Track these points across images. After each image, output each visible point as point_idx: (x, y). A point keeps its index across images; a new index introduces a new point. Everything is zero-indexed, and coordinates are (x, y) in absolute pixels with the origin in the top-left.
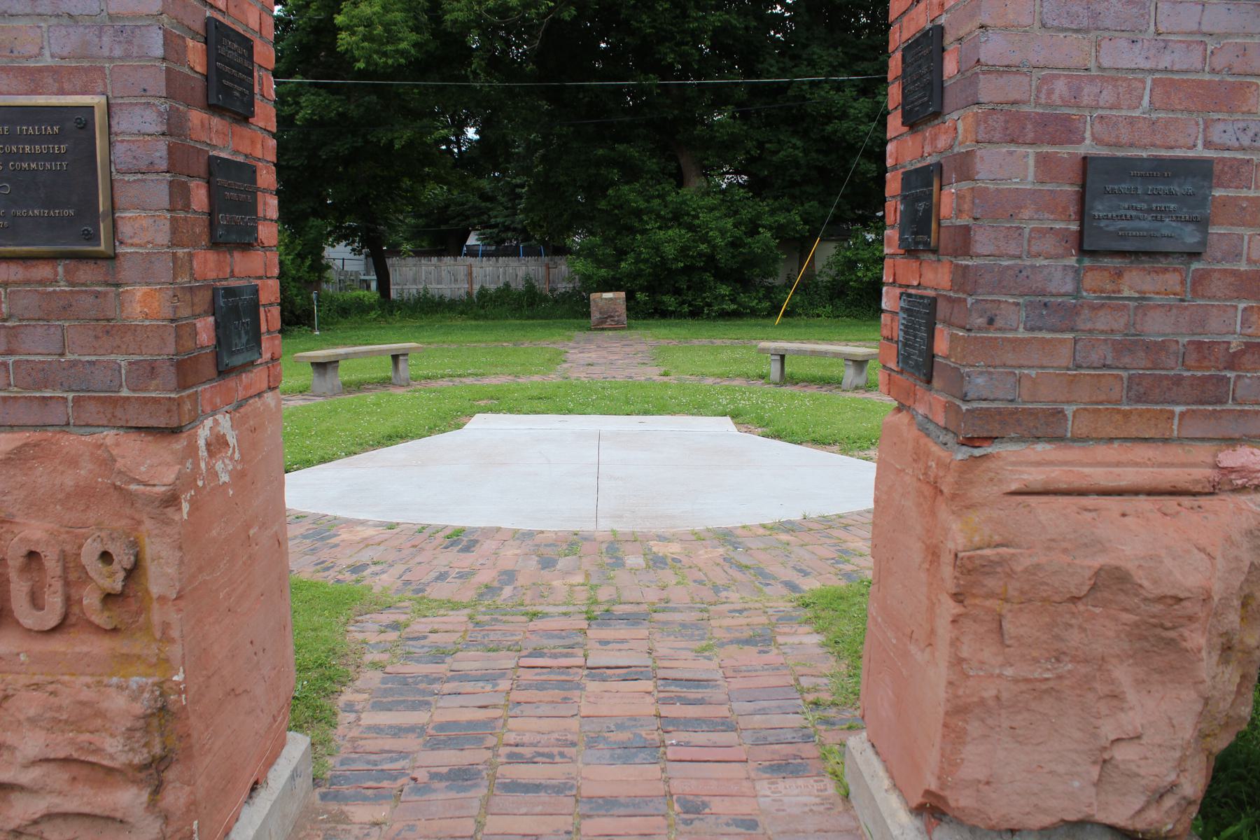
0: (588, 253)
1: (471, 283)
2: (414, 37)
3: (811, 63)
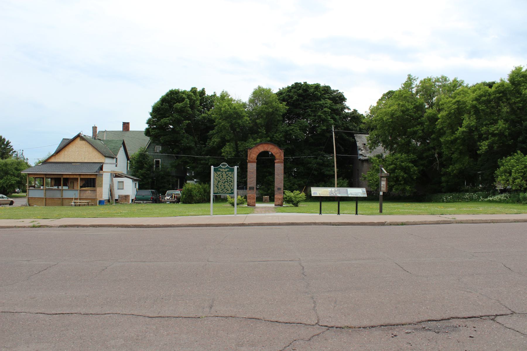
2: (234, 153)
3: (304, 153)
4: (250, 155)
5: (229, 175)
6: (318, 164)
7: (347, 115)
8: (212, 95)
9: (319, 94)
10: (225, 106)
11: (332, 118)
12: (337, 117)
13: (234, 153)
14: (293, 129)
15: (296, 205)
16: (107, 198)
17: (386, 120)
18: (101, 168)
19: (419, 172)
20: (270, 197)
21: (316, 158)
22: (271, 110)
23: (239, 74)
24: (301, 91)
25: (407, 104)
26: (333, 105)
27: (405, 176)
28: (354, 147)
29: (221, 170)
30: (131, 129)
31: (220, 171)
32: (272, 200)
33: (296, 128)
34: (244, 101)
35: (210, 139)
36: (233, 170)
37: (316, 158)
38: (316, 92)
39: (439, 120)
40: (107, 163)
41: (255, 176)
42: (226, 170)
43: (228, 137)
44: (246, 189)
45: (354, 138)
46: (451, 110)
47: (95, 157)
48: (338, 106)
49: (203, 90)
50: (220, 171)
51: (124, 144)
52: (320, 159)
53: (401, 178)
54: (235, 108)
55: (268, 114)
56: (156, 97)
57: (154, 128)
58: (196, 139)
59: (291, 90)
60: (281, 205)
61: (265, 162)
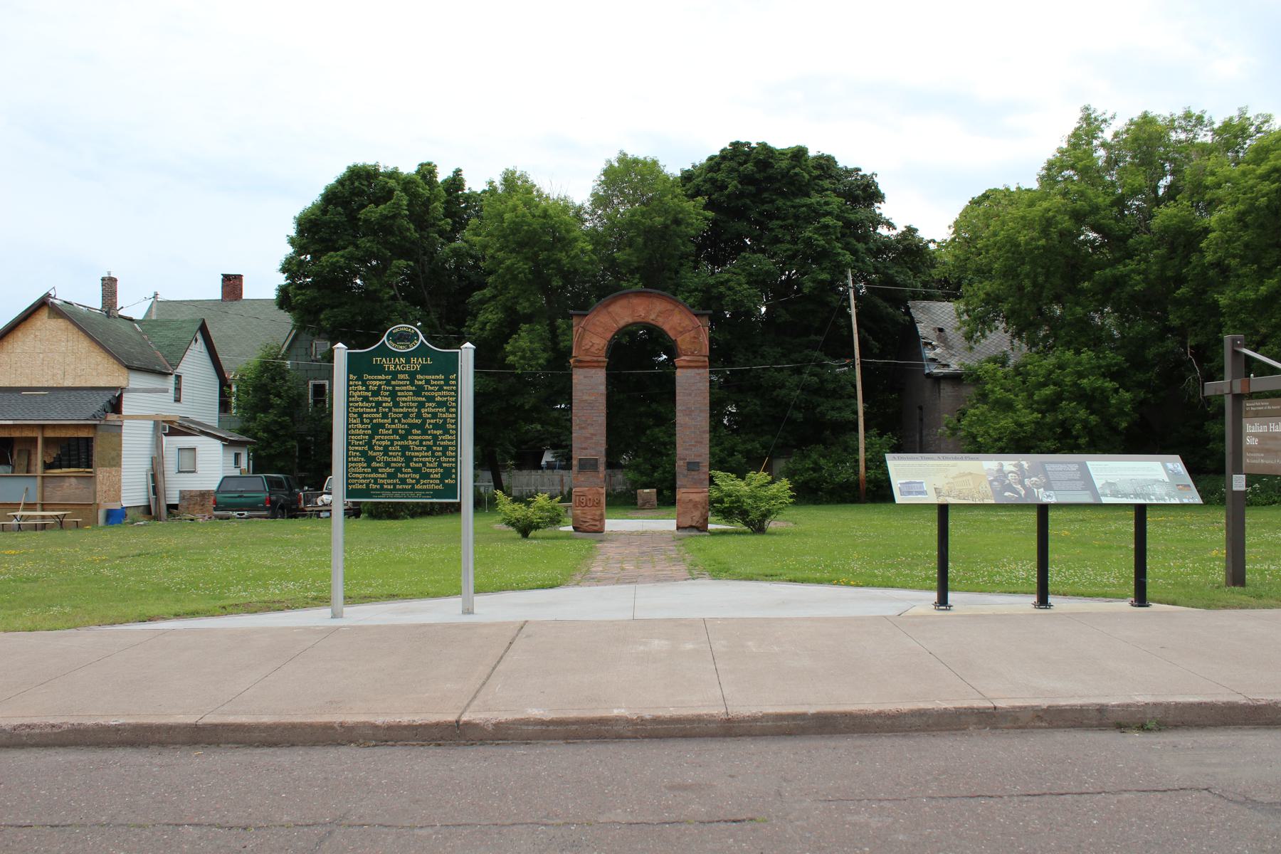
0: (636, 468)
1: (562, 485)
2: (545, 355)
3: (763, 357)
4: (582, 337)
5: (431, 390)
6: (805, 388)
7: (886, 245)
8: (484, 192)
9: (807, 176)
10: (514, 209)
11: (847, 247)
12: (861, 246)
13: (545, 355)
14: (728, 281)
15: (758, 527)
16: (143, 502)
17: (1027, 243)
18: (116, 406)
19: (1134, 409)
20: (659, 493)
21: (798, 371)
22: (659, 220)
23: (557, 112)
24: (750, 166)
25: (1090, 192)
26: (846, 211)
27: (1093, 419)
28: (908, 339)
29: (388, 364)
30: (247, 293)
31: (380, 370)
32: (667, 499)
33: (735, 278)
34: (578, 203)
35: (475, 316)
36: (450, 367)
37: (798, 371)
38: (797, 170)
39: (1212, 236)
40: (135, 390)
41: (602, 419)
42: (416, 363)
43: (527, 304)
44: (568, 467)
45: (908, 313)
46: (1257, 199)
47: (96, 370)
48: (861, 213)
49: (458, 172)
50: (380, 370)
51: (203, 329)
52: (812, 374)
53: (1078, 426)
54: (545, 215)
55: (650, 234)
56: (308, 193)
57: (300, 287)
58: (433, 316)
59: (718, 164)
60: (702, 528)
61: (639, 369)
